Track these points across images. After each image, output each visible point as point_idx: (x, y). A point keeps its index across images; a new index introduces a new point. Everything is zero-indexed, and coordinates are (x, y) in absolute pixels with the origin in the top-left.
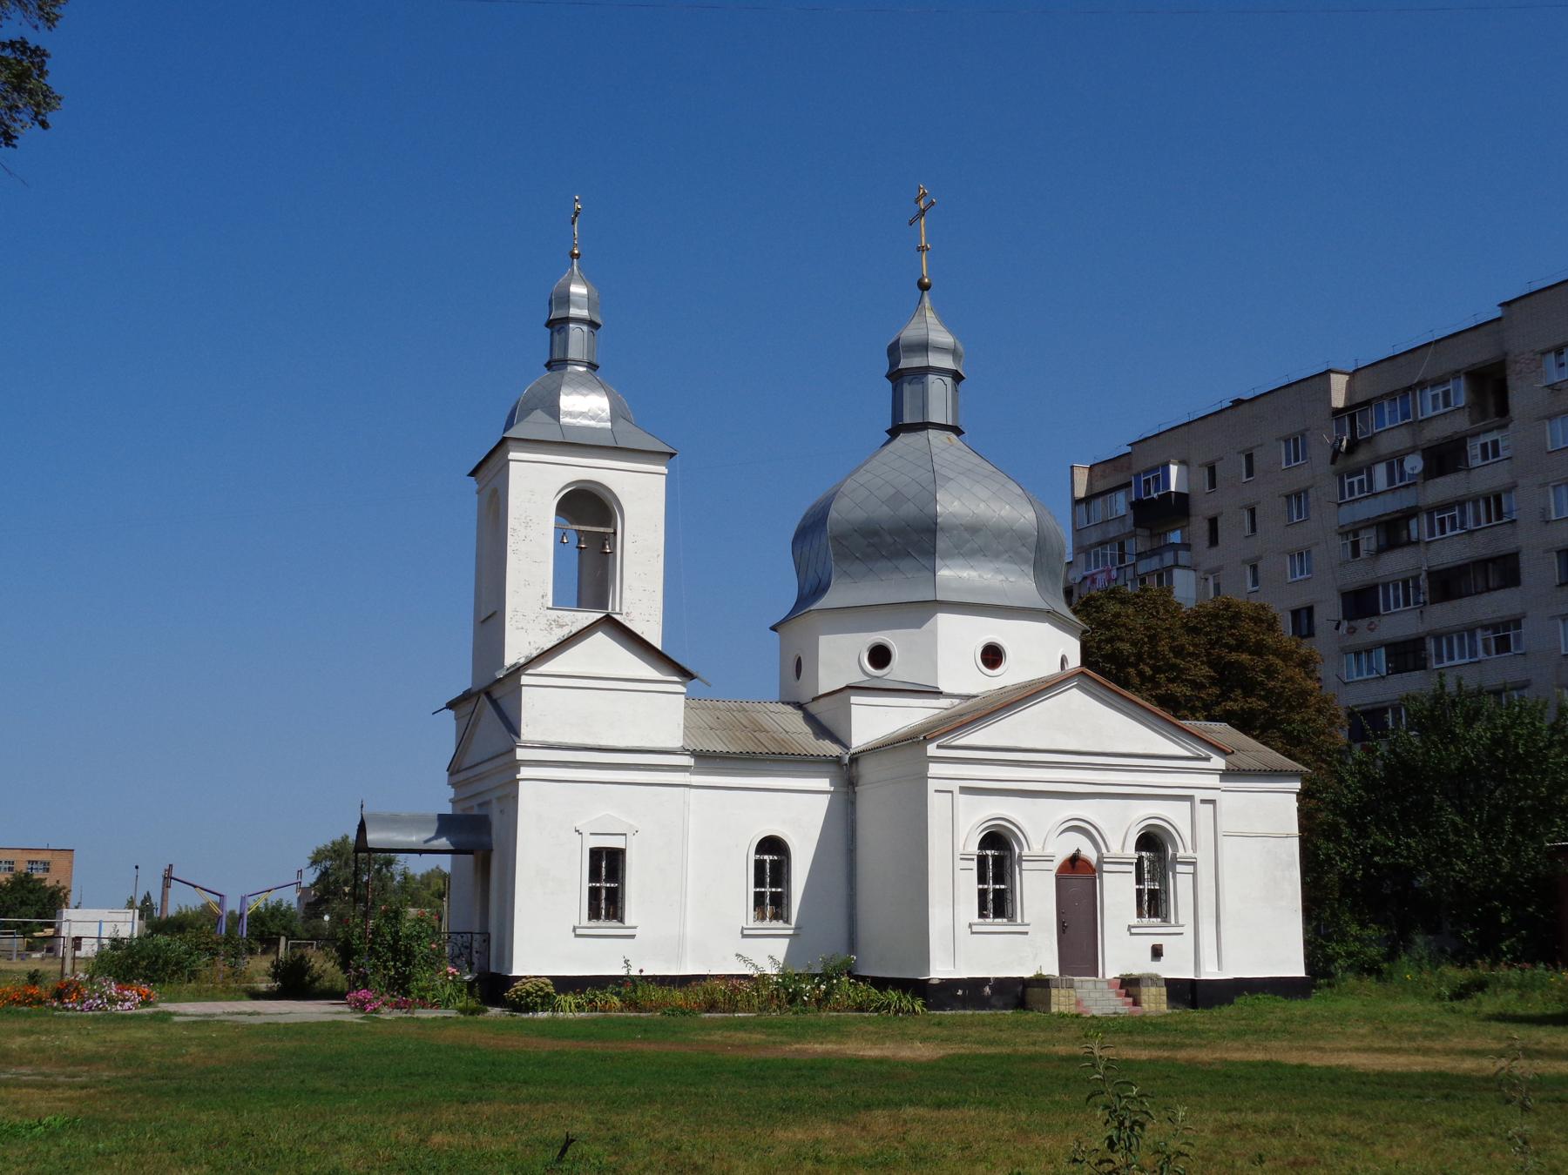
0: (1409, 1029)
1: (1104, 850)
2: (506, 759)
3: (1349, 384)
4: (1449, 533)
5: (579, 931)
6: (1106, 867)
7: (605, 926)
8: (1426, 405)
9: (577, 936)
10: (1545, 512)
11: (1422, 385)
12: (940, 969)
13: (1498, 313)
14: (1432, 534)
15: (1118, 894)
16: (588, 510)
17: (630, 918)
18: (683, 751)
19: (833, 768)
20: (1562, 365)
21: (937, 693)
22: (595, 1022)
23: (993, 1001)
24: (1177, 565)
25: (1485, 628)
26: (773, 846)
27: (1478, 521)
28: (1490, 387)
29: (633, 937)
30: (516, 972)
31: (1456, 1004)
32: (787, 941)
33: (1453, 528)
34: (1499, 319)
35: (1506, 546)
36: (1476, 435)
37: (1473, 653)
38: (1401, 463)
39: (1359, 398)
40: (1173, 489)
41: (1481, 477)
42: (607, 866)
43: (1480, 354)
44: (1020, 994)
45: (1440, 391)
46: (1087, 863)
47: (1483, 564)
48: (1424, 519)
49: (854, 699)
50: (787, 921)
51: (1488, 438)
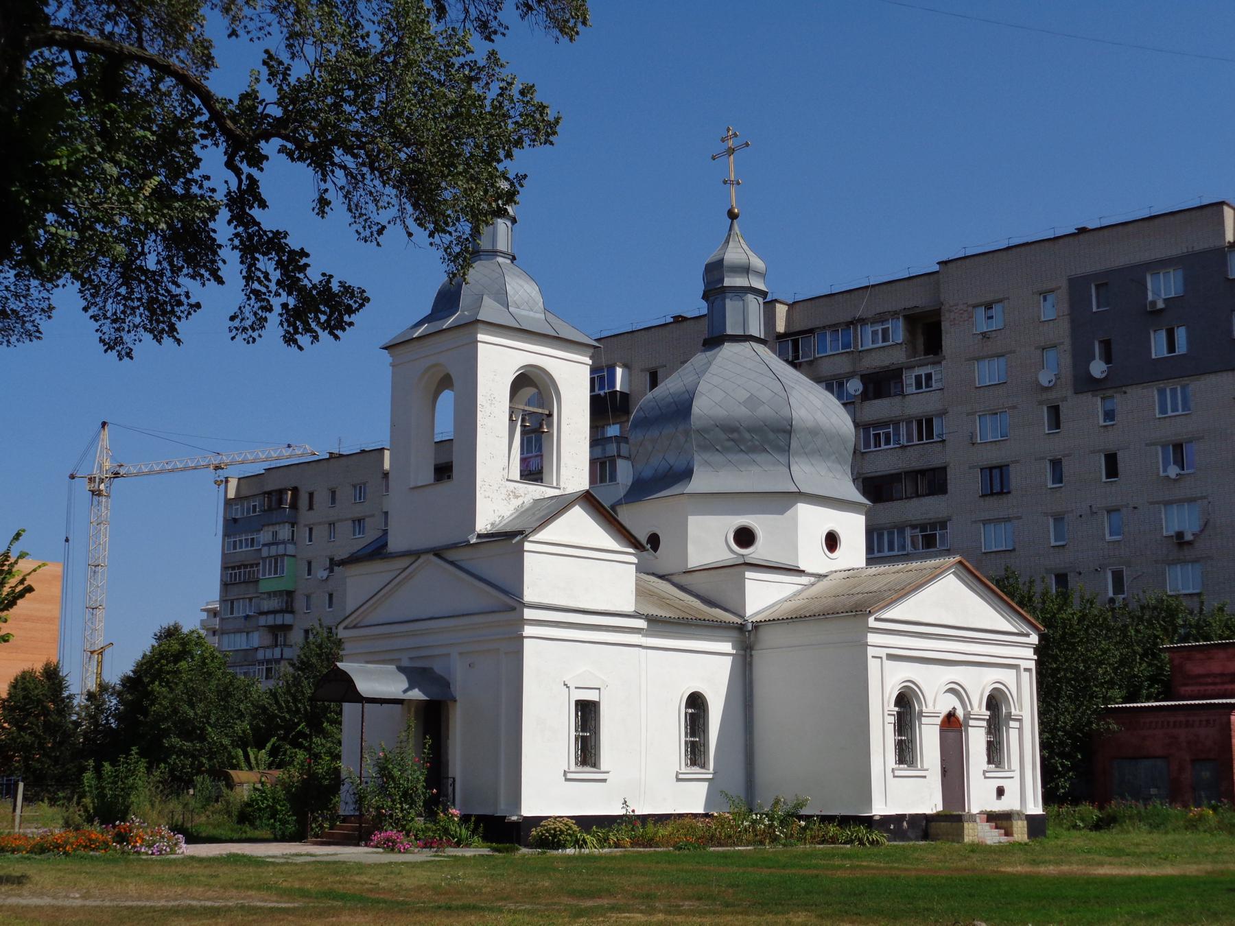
0: (1150, 852)
3: (788, 311)
4: (883, 447)
5: (570, 776)
6: (971, 723)
7: (904, 770)
8: (867, 338)
9: (567, 780)
11: (862, 321)
12: (879, 809)
13: (937, 268)
15: (977, 739)
16: (531, 389)
17: (604, 767)
18: (636, 615)
19: (735, 634)
20: (992, 317)
21: (801, 572)
24: (619, 456)
25: (914, 527)
26: (696, 702)
27: (910, 439)
28: (927, 331)
29: (604, 781)
31: (1093, 834)
32: (706, 784)
35: (936, 462)
36: (911, 367)
37: (903, 547)
38: (841, 385)
39: (797, 328)
40: (618, 388)
41: (915, 403)
42: (587, 712)
43: (918, 300)
44: (922, 826)
45: (879, 328)
46: (958, 719)
47: (915, 475)
49: (748, 574)
50: (703, 766)
51: (922, 371)
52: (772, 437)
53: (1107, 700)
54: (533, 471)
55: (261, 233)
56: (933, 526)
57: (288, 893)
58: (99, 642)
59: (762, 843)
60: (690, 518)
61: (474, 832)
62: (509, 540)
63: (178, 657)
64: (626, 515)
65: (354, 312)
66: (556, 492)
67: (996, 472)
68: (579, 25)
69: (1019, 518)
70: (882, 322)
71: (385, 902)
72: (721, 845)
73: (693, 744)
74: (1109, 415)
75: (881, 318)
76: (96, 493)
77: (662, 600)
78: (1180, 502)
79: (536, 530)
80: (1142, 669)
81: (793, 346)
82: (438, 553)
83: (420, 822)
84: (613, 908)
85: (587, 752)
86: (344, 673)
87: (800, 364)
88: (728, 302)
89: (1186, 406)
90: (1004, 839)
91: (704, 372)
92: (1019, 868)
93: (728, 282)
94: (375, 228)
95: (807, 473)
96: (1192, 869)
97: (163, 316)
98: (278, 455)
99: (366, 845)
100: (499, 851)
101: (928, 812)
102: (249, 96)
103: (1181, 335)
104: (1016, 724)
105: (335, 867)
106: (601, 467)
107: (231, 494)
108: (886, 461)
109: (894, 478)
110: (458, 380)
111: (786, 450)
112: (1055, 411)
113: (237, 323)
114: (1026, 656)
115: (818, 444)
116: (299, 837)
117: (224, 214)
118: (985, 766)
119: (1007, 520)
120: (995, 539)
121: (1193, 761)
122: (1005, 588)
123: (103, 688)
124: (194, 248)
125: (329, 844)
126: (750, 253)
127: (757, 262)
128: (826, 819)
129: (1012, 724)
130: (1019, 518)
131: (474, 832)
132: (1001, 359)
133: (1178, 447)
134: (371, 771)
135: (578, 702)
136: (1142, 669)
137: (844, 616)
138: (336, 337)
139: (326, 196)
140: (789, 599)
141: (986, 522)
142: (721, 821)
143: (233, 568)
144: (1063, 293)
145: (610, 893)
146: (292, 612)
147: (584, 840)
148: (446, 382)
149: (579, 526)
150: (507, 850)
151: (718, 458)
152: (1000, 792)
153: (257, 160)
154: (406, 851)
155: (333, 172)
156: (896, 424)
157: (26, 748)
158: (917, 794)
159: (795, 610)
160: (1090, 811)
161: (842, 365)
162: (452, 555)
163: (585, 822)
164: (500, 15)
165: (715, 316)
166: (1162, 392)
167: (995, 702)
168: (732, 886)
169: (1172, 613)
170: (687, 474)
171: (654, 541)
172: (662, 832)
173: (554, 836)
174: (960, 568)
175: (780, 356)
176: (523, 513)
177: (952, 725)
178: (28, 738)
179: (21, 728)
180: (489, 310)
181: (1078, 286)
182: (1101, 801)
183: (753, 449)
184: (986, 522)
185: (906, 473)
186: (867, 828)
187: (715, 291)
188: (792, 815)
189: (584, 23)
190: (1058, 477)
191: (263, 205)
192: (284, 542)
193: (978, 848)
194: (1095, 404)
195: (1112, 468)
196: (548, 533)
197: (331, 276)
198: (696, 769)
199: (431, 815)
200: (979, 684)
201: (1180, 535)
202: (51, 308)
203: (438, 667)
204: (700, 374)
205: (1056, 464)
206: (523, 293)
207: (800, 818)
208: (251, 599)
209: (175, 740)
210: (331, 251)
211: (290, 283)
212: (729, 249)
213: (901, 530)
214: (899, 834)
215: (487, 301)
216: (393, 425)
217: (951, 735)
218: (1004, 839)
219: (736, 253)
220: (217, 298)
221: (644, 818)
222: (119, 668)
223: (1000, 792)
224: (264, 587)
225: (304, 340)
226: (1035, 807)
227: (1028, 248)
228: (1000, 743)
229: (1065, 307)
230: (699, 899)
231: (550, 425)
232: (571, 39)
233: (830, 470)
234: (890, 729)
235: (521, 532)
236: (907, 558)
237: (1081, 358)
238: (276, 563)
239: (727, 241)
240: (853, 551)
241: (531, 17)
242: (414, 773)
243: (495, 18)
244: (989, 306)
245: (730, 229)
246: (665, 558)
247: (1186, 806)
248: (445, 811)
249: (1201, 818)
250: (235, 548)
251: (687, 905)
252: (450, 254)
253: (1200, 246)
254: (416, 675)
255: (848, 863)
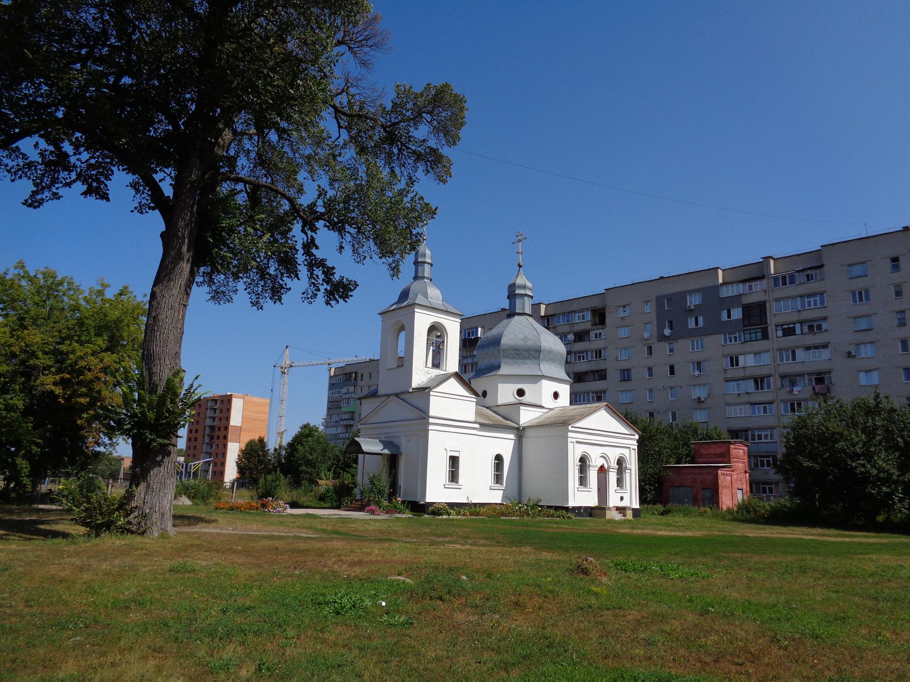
2: (424, 421)
7: (454, 485)
8: (576, 318)
10: (617, 357)
11: (575, 312)
12: (572, 504)
15: (613, 477)
16: (436, 332)
22: (460, 520)
26: (499, 458)
27: (592, 357)
28: (600, 316)
35: (602, 367)
38: (566, 336)
41: (595, 344)
42: (454, 461)
43: (597, 304)
44: (589, 512)
47: (593, 372)
48: (573, 355)
51: (598, 332)
52: (533, 353)
53: (667, 462)
54: (436, 365)
55: (316, 259)
56: (601, 392)
57: (317, 531)
58: (283, 430)
60: (500, 385)
61: (407, 507)
62: (424, 391)
63: (307, 436)
74: (671, 350)
75: (582, 311)
76: (283, 373)
78: (699, 385)
79: (435, 387)
80: (683, 451)
81: (548, 321)
82: (397, 395)
83: (385, 503)
85: (454, 476)
89: (702, 347)
95: (546, 368)
96: (698, 534)
97: (277, 293)
98: (352, 359)
102: (314, 204)
103: (700, 319)
105: (343, 520)
106: (463, 365)
107: (332, 374)
108: (582, 366)
109: (586, 373)
110: (406, 328)
111: (538, 358)
112: (650, 348)
113: (305, 295)
114: (634, 444)
115: (551, 356)
116: (338, 507)
117: (301, 251)
119: (630, 391)
120: (625, 398)
121: (703, 489)
122: (627, 417)
123: (280, 447)
124: (288, 265)
127: (529, 284)
128: (550, 507)
131: (407, 507)
133: (699, 364)
134: (366, 480)
136: (683, 451)
137: (560, 425)
141: (622, 391)
144: (654, 302)
145: (451, 535)
148: (402, 328)
149: (453, 386)
151: (511, 361)
152: (622, 498)
153: (314, 229)
156: (587, 352)
157: (250, 469)
158: (589, 499)
160: (660, 507)
161: (566, 329)
162: (403, 396)
163: (452, 505)
165: (513, 304)
166: (693, 342)
167: (620, 462)
169: (696, 430)
171: (485, 394)
176: (431, 380)
177: (602, 470)
178: (252, 466)
179: (249, 462)
180: (420, 299)
181: (659, 299)
182: (664, 503)
183: (525, 358)
184: (622, 391)
187: (512, 295)
190: (651, 374)
191: (317, 248)
193: (612, 522)
194: (666, 346)
195: (672, 370)
196: (440, 389)
199: (390, 501)
200: (614, 455)
201: (699, 398)
202: (237, 290)
203: (395, 441)
205: (650, 369)
206: (434, 294)
209: (304, 468)
210: (344, 266)
211: (328, 280)
213: (588, 394)
215: (419, 296)
219: (521, 281)
220: (298, 285)
221: (475, 504)
222: (287, 439)
223: (622, 498)
224: (343, 410)
225: (333, 303)
226: (636, 505)
228: (622, 478)
229: (654, 308)
234: (577, 472)
236: (589, 402)
237: (661, 327)
240: (565, 399)
244: (624, 307)
246: (488, 400)
247: (699, 507)
249: (705, 512)
251: (481, 542)
253: (709, 284)
254: (386, 444)
255: (555, 526)
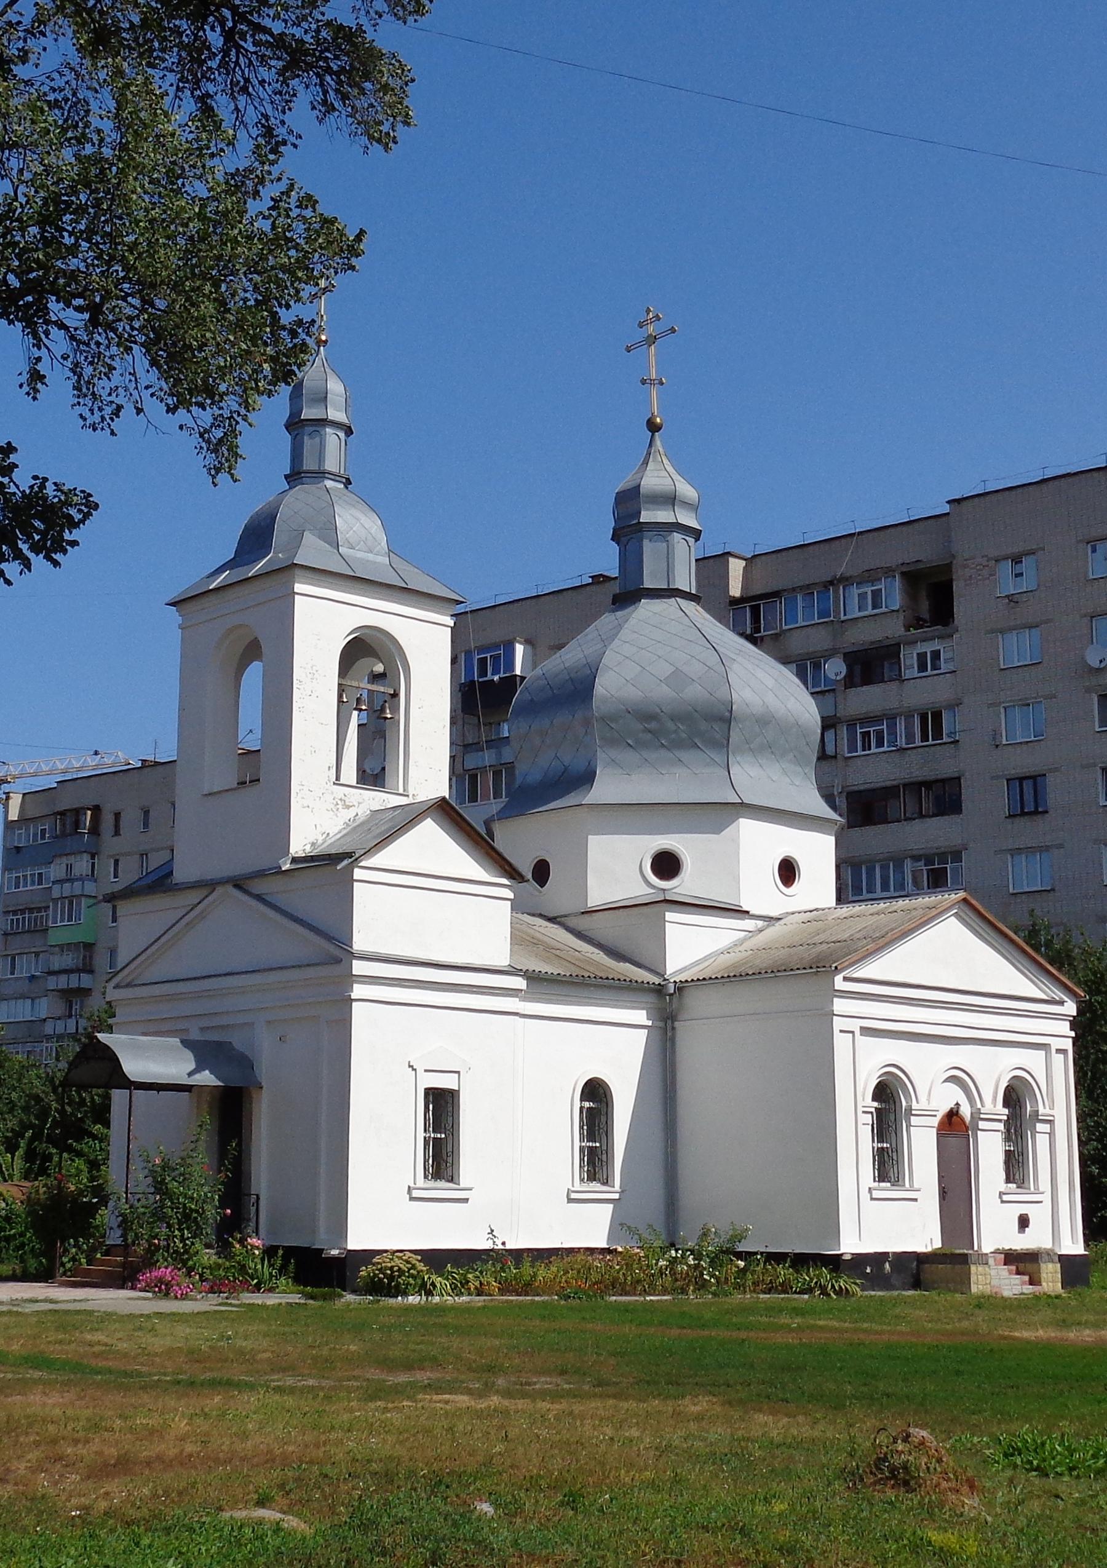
1: (979, 1106)
2: (336, 970)
4: (874, 750)
5: (415, 1193)
6: (982, 1125)
7: (885, 1190)
8: (852, 603)
9: (412, 1199)
10: (996, 734)
11: (846, 581)
12: (850, 1245)
13: (946, 509)
14: (852, 748)
15: (990, 1149)
17: (465, 1179)
19: (651, 998)
22: (467, 1310)
23: (893, 1281)
25: (916, 858)
26: (596, 1093)
27: (910, 738)
28: (933, 594)
29: (466, 1200)
30: (356, 1242)
33: (880, 744)
34: (948, 514)
38: (817, 666)
40: (518, 672)
41: (917, 691)
42: (442, 1106)
43: (921, 551)
44: (912, 1270)
45: (868, 590)
46: (962, 1120)
47: (916, 787)
48: (844, 731)
49: (669, 916)
51: (928, 648)
52: (703, 728)
56: (943, 857)
59: (684, 1291)
60: (594, 841)
61: (283, 1270)
62: (334, 866)
64: (505, 838)
65: (76, 525)
66: (403, 801)
67: (1028, 786)
68: (399, 126)
69: (1060, 846)
70: (873, 582)
71: (110, 1372)
72: (627, 1294)
73: (592, 1151)
75: (870, 576)
77: (550, 951)
79: (369, 852)
81: (753, 616)
82: (239, 883)
83: (208, 1256)
84: (429, 1387)
85: (441, 1159)
86: (107, 1048)
87: (762, 638)
88: (646, 543)
90: (1028, 1289)
91: (613, 638)
92: (1041, 1333)
93: (646, 516)
94: (108, 410)
95: (753, 777)
98: (80, 762)
99: (133, 1288)
100: (312, 1298)
101: (921, 1248)
104: (1045, 1127)
107: (13, 815)
108: (876, 769)
109: (890, 792)
110: (264, 649)
115: (769, 737)
116: (44, 1276)
118: (1003, 1186)
119: (1044, 849)
120: (1026, 875)
122: (1038, 943)
125: (75, 1285)
126: (676, 477)
127: (686, 490)
129: (1040, 1127)
130: (1060, 846)
131: (283, 1270)
132: (1033, 630)
134: (141, 1180)
135: (428, 1091)
137: (805, 971)
138: (56, 563)
139: (41, 367)
140: (727, 951)
141: (1016, 852)
142: (628, 1260)
143: (15, 913)
145: (436, 1363)
146: (91, 971)
147: (433, 1284)
148: (252, 651)
149: (433, 847)
150: (325, 1297)
151: (630, 756)
152: (1024, 1222)
154: (184, 1297)
155: (47, 333)
156: (892, 718)
159: (734, 966)
161: (819, 640)
162: (259, 887)
163: (436, 1259)
164: (287, 118)
167: (1015, 1096)
168: (614, 1354)
170: (587, 778)
171: (542, 872)
172: (542, 1273)
173: (391, 1278)
174: (966, 909)
175: (734, 630)
176: (357, 828)
177: (954, 1128)
183: (678, 744)
184: (1016, 852)
185: (905, 785)
186: (831, 1271)
187: (629, 531)
188: (727, 1252)
189: (406, 123)
192: (81, 879)
193: (990, 1302)
197: (45, 479)
198: (596, 1186)
199: (224, 1248)
200: (992, 1071)
203: (237, 1041)
204: (606, 642)
206: (360, 530)
207: (739, 1255)
208: (37, 954)
212: (647, 472)
214: (878, 1280)
215: (310, 539)
216: (181, 709)
217: (953, 1141)
218: (1028, 1289)
219: (658, 476)
221: (518, 1255)
223: (1024, 1222)
224: (56, 937)
226: (1073, 1245)
227: (1070, 480)
228: (1023, 1153)
230: (563, 1372)
231: (395, 709)
232: (386, 148)
233: (785, 772)
234: (866, 1133)
235: (349, 855)
238: (71, 903)
239: (646, 462)
240: (819, 884)
241: (331, 118)
242: (202, 1187)
243: (283, 122)
244: (1017, 560)
245: (650, 445)
246: (556, 894)
248: (242, 1241)
250: (17, 887)
251: (542, 1382)
252: (208, 442)
254: (207, 1052)
